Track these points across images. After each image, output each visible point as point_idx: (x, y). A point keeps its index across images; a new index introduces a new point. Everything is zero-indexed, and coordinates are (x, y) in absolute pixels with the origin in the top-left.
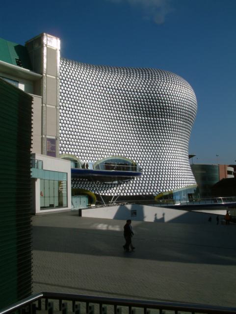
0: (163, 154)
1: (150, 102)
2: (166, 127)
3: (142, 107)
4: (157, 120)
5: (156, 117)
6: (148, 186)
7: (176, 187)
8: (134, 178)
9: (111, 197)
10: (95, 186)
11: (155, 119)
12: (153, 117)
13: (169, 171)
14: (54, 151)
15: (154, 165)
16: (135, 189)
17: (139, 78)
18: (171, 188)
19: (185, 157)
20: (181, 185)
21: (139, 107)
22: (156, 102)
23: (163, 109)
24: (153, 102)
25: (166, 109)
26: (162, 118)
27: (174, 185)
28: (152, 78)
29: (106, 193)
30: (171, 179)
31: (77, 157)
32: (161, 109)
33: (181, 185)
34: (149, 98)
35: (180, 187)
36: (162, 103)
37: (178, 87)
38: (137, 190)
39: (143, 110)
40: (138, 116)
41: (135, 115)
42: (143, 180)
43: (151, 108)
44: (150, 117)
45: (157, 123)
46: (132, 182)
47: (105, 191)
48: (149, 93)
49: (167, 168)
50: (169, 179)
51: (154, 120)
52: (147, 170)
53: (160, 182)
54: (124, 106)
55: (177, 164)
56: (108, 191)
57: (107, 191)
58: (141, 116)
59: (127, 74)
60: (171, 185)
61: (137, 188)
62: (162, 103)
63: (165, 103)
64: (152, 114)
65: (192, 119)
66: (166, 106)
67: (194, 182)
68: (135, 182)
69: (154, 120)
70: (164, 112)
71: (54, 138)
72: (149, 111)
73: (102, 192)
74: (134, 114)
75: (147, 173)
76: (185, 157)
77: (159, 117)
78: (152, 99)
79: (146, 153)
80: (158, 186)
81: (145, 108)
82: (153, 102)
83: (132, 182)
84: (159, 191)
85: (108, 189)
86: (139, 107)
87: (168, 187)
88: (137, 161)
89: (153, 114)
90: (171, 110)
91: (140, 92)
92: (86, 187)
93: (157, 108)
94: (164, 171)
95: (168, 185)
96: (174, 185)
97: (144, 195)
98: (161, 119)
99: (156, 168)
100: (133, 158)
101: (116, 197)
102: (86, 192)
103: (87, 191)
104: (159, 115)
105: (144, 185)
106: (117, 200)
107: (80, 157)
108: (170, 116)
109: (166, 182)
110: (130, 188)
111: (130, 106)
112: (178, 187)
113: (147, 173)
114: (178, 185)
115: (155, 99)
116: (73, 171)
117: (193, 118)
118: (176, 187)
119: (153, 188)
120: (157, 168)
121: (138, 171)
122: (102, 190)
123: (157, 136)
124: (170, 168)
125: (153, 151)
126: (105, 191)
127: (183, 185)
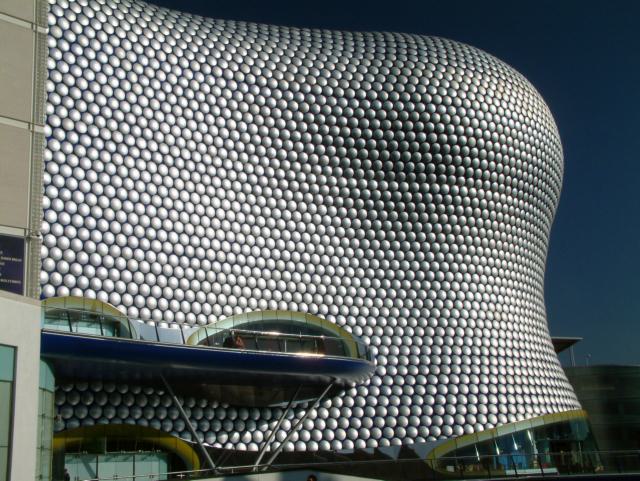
0: (450, 304)
1: (395, 129)
2: (456, 213)
3: (368, 147)
4: (422, 190)
5: (419, 180)
6: (356, 404)
7: (504, 419)
8: (348, 388)
9: (256, 455)
10: (181, 417)
11: (417, 186)
12: (408, 180)
13: (478, 361)
14: (530, 435)
15: (420, 341)
16: (352, 426)
17: (355, 54)
18: (484, 420)
19: (533, 286)
20: (521, 409)
21: (358, 146)
22: (416, 130)
23: (443, 152)
24: (405, 129)
25: (453, 153)
26: (440, 181)
27: (495, 409)
28: (397, 54)
29: (241, 440)
30: (485, 390)
31: (122, 309)
32: (433, 151)
33: (521, 409)
34: (389, 117)
35: (521, 418)
36: (437, 131)
37: (490, 84)
38: (323, 431)
39: (371, 157)
40: (356, 176)
41: (346, 175)
42: (382, 393)
43: (401, 149)
44: (398, 179)
45: (445, 202)
46: (340, 402)
47: (236, 435)
48: (391, 99)
49: (469, 351)
50: (476, 390)
51: (411, 190)
52: (396, 361)
53: (443, 400)
54: (305, 144)
55: (513, 339)
56: (248, 435)
57: (242, 434)
58: (367, 177)
59: (312, 42)
60: (474, 410)
61: (359, 423)
62: (437, 131)
63: (447, 132)
64: (405, 173)
65: (548, 205)
66: (450, 142)
67: (569, 402)
68: (352, 402)
69: (411, 190)
70: (444, 161)
71: (19, 233)
72: (393, 158)
73: (225, 437)
74: (340, 170)
75: (395, 371)
76: (533, 286)
77: (429, 181)
78: (400, 118)
79: (378, 282)
80: (435, 413)
81: (379, 148)
82: (405, 129)
83: (340, 402)
84: (443, 434)
85: (246, 430)
86: (358, 146)
87: (474, 420)
88: (360, 331)
89: (407, 170)
90: (472, 156)
91: (357, 97)
92: (156, 417)
93: (422, 150)
94: (485, 400)
95: (474, 410)
96: (495, 409)
97: (302, 453)
98: (437, 186)
99: (429, 351)
100: (343, 320)
101: (268, 455)
102: (155, 440)
103: (162, 433)
104: (427, 171)
105: (385, 411)
106: (275, 462)
107: (134, 311)
108: (466, 176)
109: (475, 400)
110: (335, 424)
111: (325, 143)
112: (513, 419)
113: (395, 371)
114: (513, 409)
115: (411, 119)
116: (53, 348)
117: (544, 226)
118: (504, 419)
119: (406, 421)
120: (443, 354)
121: (353, 358)
122: (223, 430)
123: (428, 245)
124: (478, 352)
125: (414, 294)
126: (236, 435)
127: (529, 409)
